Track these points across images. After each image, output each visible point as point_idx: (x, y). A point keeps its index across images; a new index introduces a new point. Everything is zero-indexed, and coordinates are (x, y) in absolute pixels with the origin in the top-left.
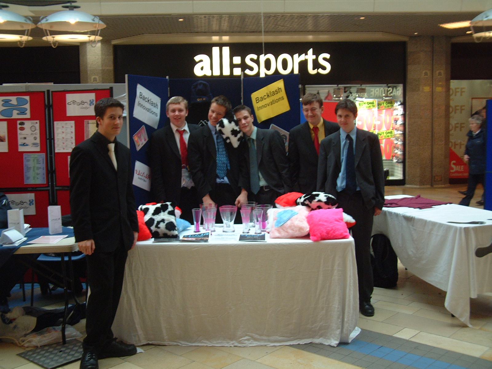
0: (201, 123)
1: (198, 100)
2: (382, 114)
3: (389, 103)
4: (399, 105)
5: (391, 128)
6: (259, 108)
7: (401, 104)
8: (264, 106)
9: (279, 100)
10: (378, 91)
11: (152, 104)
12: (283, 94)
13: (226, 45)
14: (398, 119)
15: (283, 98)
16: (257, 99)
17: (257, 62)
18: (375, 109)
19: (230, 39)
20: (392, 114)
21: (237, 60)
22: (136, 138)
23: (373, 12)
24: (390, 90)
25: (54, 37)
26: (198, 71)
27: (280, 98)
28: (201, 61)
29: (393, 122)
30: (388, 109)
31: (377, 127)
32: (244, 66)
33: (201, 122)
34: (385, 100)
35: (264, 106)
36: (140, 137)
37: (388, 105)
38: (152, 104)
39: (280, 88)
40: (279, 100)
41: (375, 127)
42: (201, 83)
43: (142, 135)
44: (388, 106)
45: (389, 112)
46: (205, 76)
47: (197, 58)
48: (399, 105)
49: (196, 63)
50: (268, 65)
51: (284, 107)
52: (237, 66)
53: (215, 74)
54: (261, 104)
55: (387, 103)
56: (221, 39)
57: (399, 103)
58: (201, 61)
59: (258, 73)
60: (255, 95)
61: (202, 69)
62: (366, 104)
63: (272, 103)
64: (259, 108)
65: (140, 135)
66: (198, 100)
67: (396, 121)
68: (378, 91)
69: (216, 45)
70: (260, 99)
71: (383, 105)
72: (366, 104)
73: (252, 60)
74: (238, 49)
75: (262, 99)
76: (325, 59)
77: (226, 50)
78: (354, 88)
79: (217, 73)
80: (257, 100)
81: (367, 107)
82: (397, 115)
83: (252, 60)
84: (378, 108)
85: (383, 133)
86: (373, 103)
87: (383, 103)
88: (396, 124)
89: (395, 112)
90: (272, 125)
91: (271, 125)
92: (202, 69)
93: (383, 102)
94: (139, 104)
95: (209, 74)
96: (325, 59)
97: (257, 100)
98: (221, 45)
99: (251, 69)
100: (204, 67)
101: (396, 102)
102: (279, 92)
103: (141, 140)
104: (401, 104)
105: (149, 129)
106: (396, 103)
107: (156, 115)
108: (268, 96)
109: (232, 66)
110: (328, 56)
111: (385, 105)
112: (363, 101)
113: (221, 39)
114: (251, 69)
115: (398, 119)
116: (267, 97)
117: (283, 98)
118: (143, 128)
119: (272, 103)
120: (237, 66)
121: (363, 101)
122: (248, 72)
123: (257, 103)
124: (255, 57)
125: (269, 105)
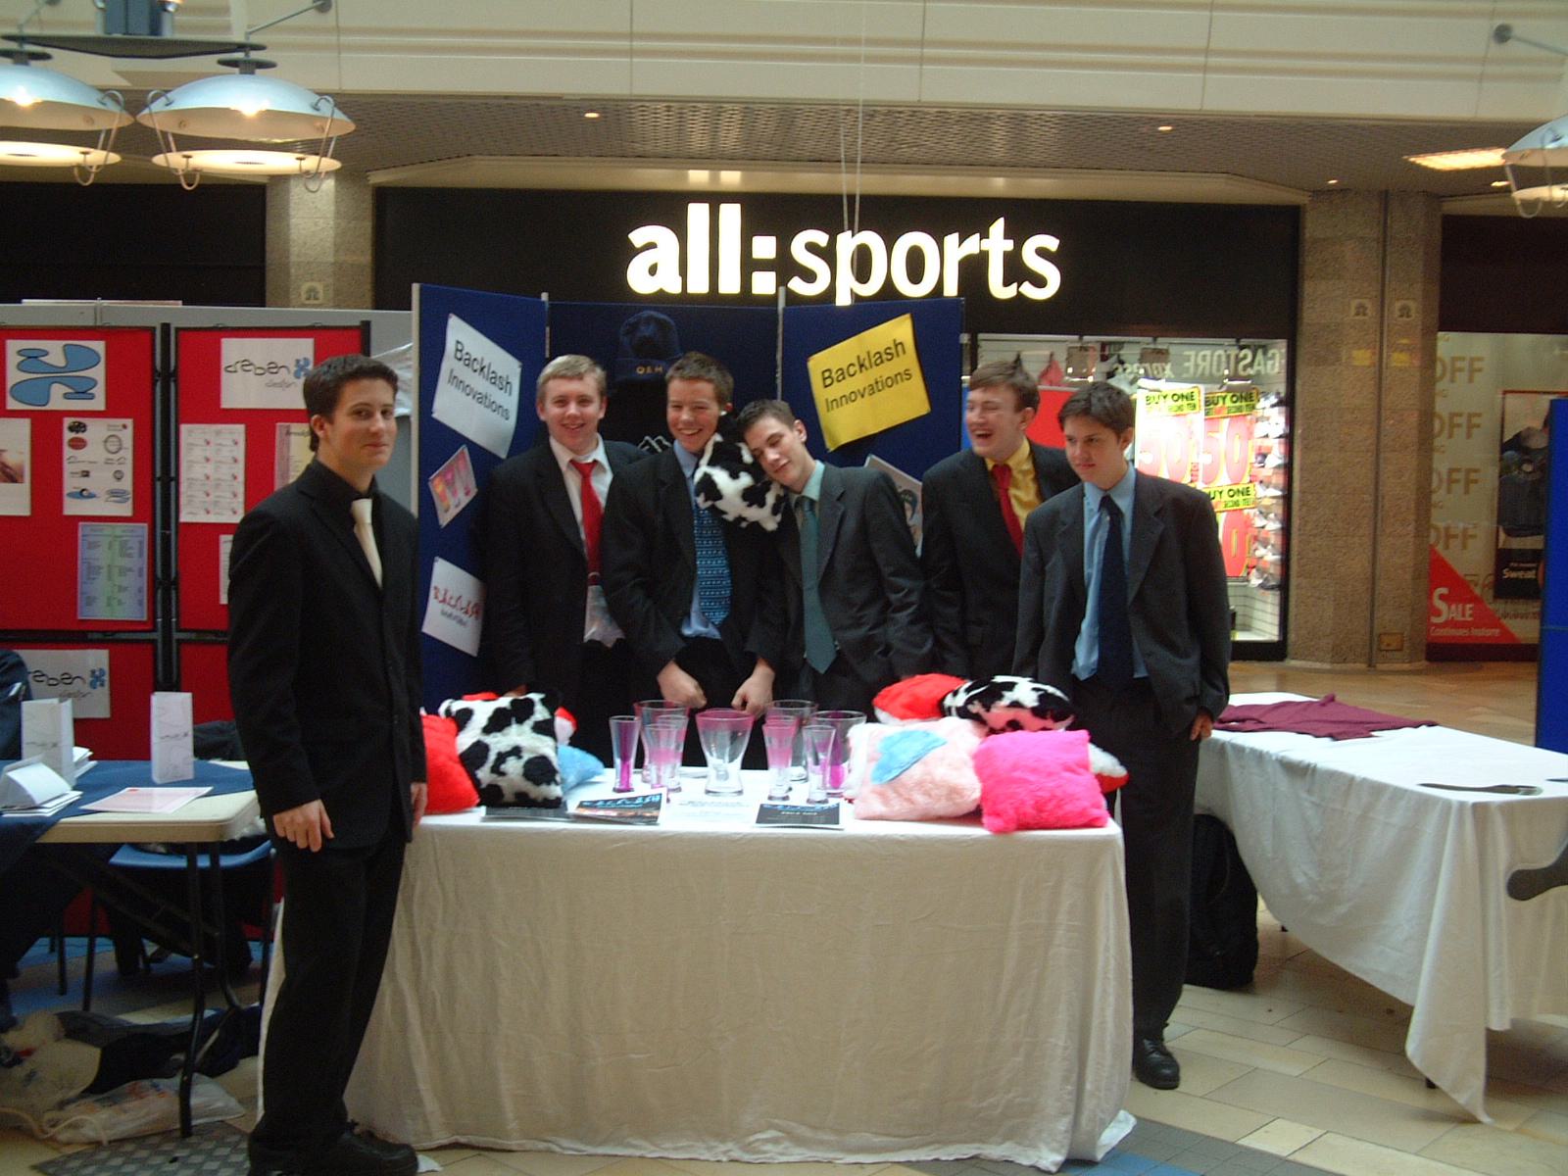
0: (647, 443)
1: (640, 371)
2: (1217, 432)
3: (1241, 398)
4: (1273, 406)
5: (1247, 479)
6: (833, 404)
7: (1279, 404)
8: (849, 398)
9: (894, 380)
10: (1208, 358)
11: (495, 379)
12: (909, 360)
13: (730, 197)
14: (1270, 450)
15: (908, 375)
16: (827, 374)
17: (828, 255)
18: (1198, 417)
19: (744, 180)
20: (1250, 435)
21: (765, 247)
22: (437, 487)
23: (1200, 110)
24: (1245, 357)
25: (189, 157)
26: (639, 279)
27: (899, 374)
28: (651, 246)
29: (1252, 458)
30: (1237, 417)
31: (1201, 474)
32: (785, 266)
33: (647, 442)
34: (1230, 389)
35: (849, 398)
36: (450, 484)
37: (1238, 404)
38: (495, 379)
39: (901, 343)
40: (894, 380)
41: (1194, 473)
42: (649, 319)
43: (457, 477)
44: (1239, 409)
45: (1241, 426)
46: (661, 295)
47: (638, 237)
48: (1273, 406)
49: (633, 252)
50: (862, 265)
51: (909, 401)
52: (764, 265)
53: (691, 290)
54: (837, 390)
55: (1235, 399)
56: (715, 179)
57: (1273, 400)
58: (651, 246)
59: (831, 291)
60: (819, 363)
61: (653, 270)
62: (1169, 398)
63: (873, 389)
64: (833, 404)
65: (453, 476)
66: (640, 371)
67: (1263, 456)
68: (1208, 358)
69: (699, 196)
70: (834, 376)
71: (1224, 403)
72: (1169, 398)
73: (812, 248)
74: (771, 213)
75: (843, 374)
76: (1042, 252)
77: (731, 215)
78: (1132, 347)
79: (699, 285)
80: (825, 379)
81: (1170, 409)
82: (1267, 436)
83: (812, 248)
84: (1207, 414)
85: (1221, 493)
86: (1190, 397)
87: (1224, 398)
88: (1263, 467)
89: (1260, 429)
90: (872, 460)
91: (868, 459)
92: (653, 270)
93: (1223, 394)
94: (453, 378)
95: (674, 288)
96: (1042, 252)
97: (828, 378)
98: (715, 199)
99: (809, 276)
100: (657, 265)
101: (1266, 395)
102: (898, 355)
103: (454, 493)
104: (1279, 404)
105: (481, 457)
106: (1262, 400)
107: (506, 415)
108: (862, 366)
109: (750, 265)
110: (1051, 243)
111: (1228, 403)
112: (1159, 391)
113: (715, 179)
114: (809, 276)
115: (1270, 450)
116: (857, 368)
117: (908, 375)
118: (462, 452)
119: (873, 389)
120: (764, 265)
121: (1159, 391)
122: (797, 285)
123: (826, 386)
124: (821, 238)
125: (863, 396)
